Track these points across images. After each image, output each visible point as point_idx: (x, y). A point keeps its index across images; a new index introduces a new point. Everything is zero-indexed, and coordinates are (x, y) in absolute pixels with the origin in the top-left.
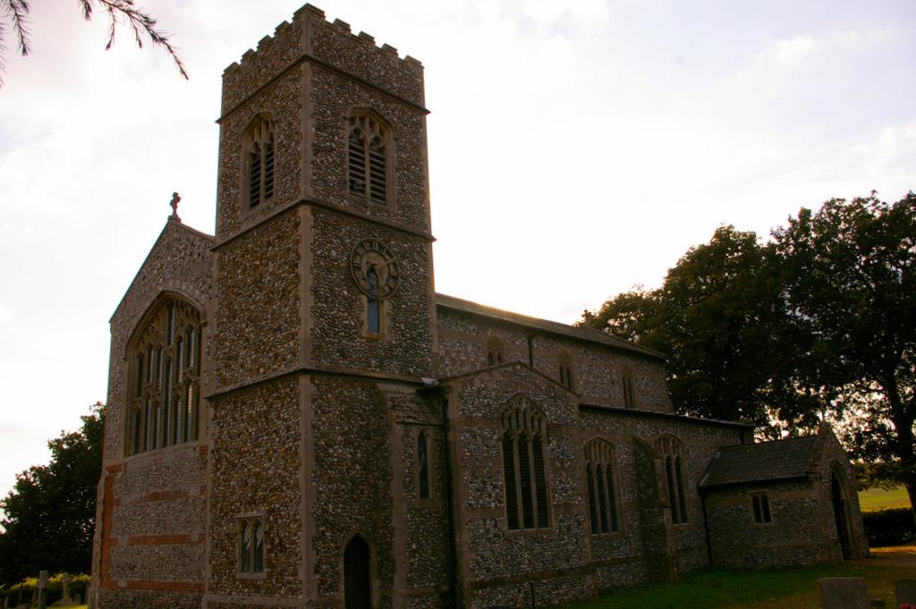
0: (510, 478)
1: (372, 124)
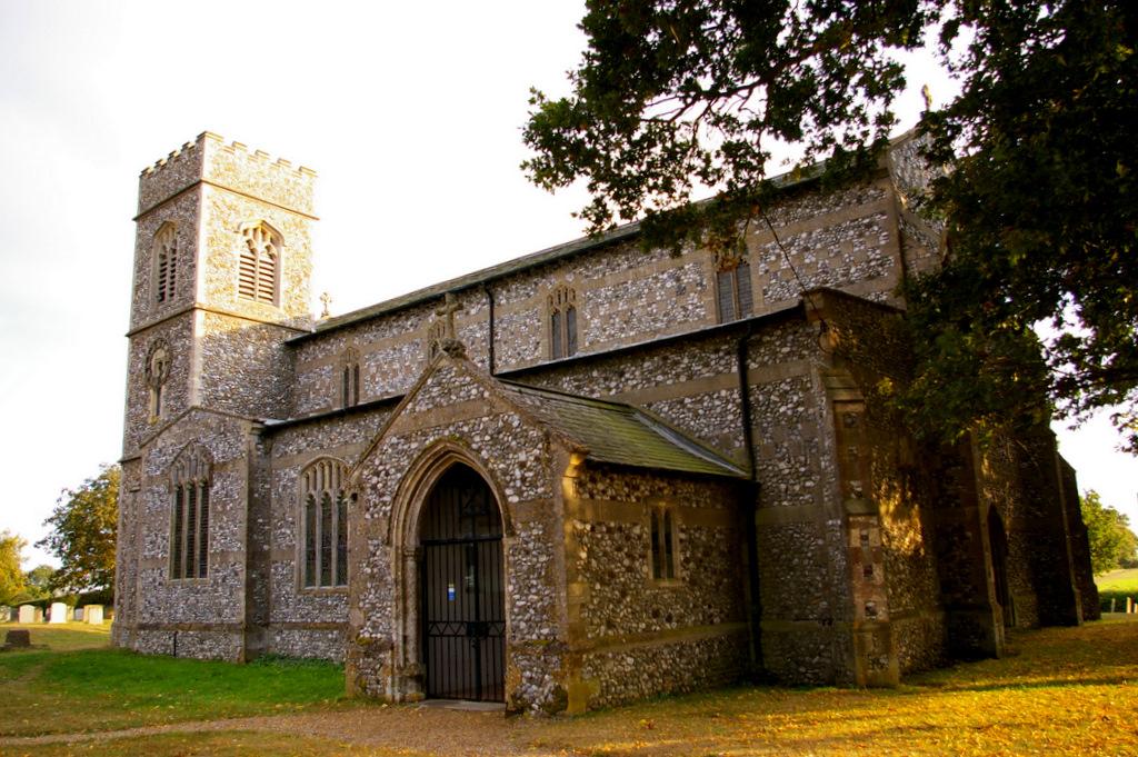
0: (178, 529)
1: (264, 233)
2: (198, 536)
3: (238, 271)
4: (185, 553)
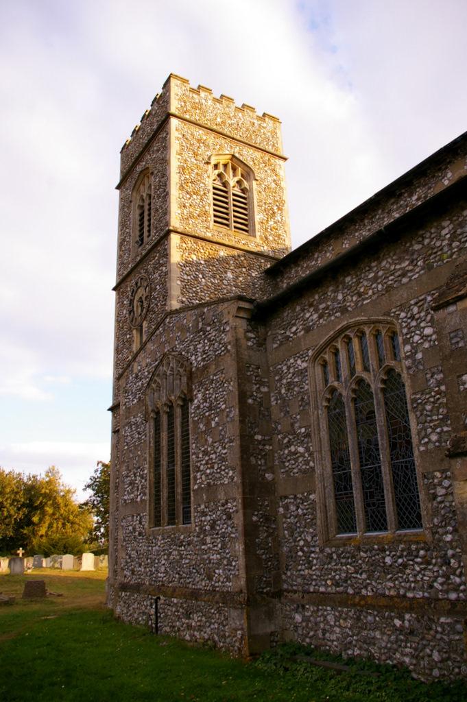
0: (157, 464)
1: (234, 169)
2: (178, 469)
3: (212, 202)
4: (165, 494)
